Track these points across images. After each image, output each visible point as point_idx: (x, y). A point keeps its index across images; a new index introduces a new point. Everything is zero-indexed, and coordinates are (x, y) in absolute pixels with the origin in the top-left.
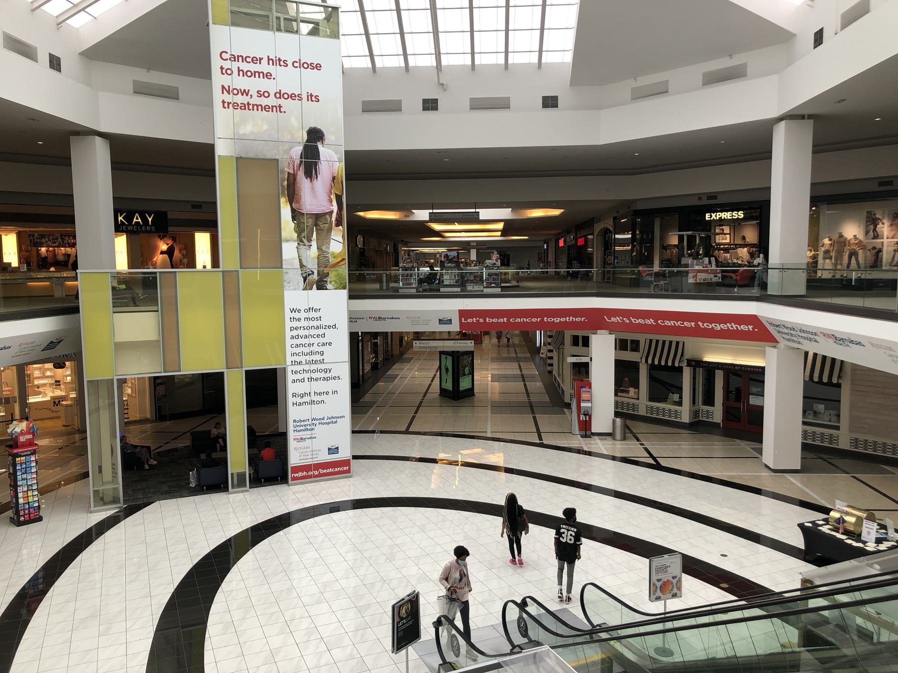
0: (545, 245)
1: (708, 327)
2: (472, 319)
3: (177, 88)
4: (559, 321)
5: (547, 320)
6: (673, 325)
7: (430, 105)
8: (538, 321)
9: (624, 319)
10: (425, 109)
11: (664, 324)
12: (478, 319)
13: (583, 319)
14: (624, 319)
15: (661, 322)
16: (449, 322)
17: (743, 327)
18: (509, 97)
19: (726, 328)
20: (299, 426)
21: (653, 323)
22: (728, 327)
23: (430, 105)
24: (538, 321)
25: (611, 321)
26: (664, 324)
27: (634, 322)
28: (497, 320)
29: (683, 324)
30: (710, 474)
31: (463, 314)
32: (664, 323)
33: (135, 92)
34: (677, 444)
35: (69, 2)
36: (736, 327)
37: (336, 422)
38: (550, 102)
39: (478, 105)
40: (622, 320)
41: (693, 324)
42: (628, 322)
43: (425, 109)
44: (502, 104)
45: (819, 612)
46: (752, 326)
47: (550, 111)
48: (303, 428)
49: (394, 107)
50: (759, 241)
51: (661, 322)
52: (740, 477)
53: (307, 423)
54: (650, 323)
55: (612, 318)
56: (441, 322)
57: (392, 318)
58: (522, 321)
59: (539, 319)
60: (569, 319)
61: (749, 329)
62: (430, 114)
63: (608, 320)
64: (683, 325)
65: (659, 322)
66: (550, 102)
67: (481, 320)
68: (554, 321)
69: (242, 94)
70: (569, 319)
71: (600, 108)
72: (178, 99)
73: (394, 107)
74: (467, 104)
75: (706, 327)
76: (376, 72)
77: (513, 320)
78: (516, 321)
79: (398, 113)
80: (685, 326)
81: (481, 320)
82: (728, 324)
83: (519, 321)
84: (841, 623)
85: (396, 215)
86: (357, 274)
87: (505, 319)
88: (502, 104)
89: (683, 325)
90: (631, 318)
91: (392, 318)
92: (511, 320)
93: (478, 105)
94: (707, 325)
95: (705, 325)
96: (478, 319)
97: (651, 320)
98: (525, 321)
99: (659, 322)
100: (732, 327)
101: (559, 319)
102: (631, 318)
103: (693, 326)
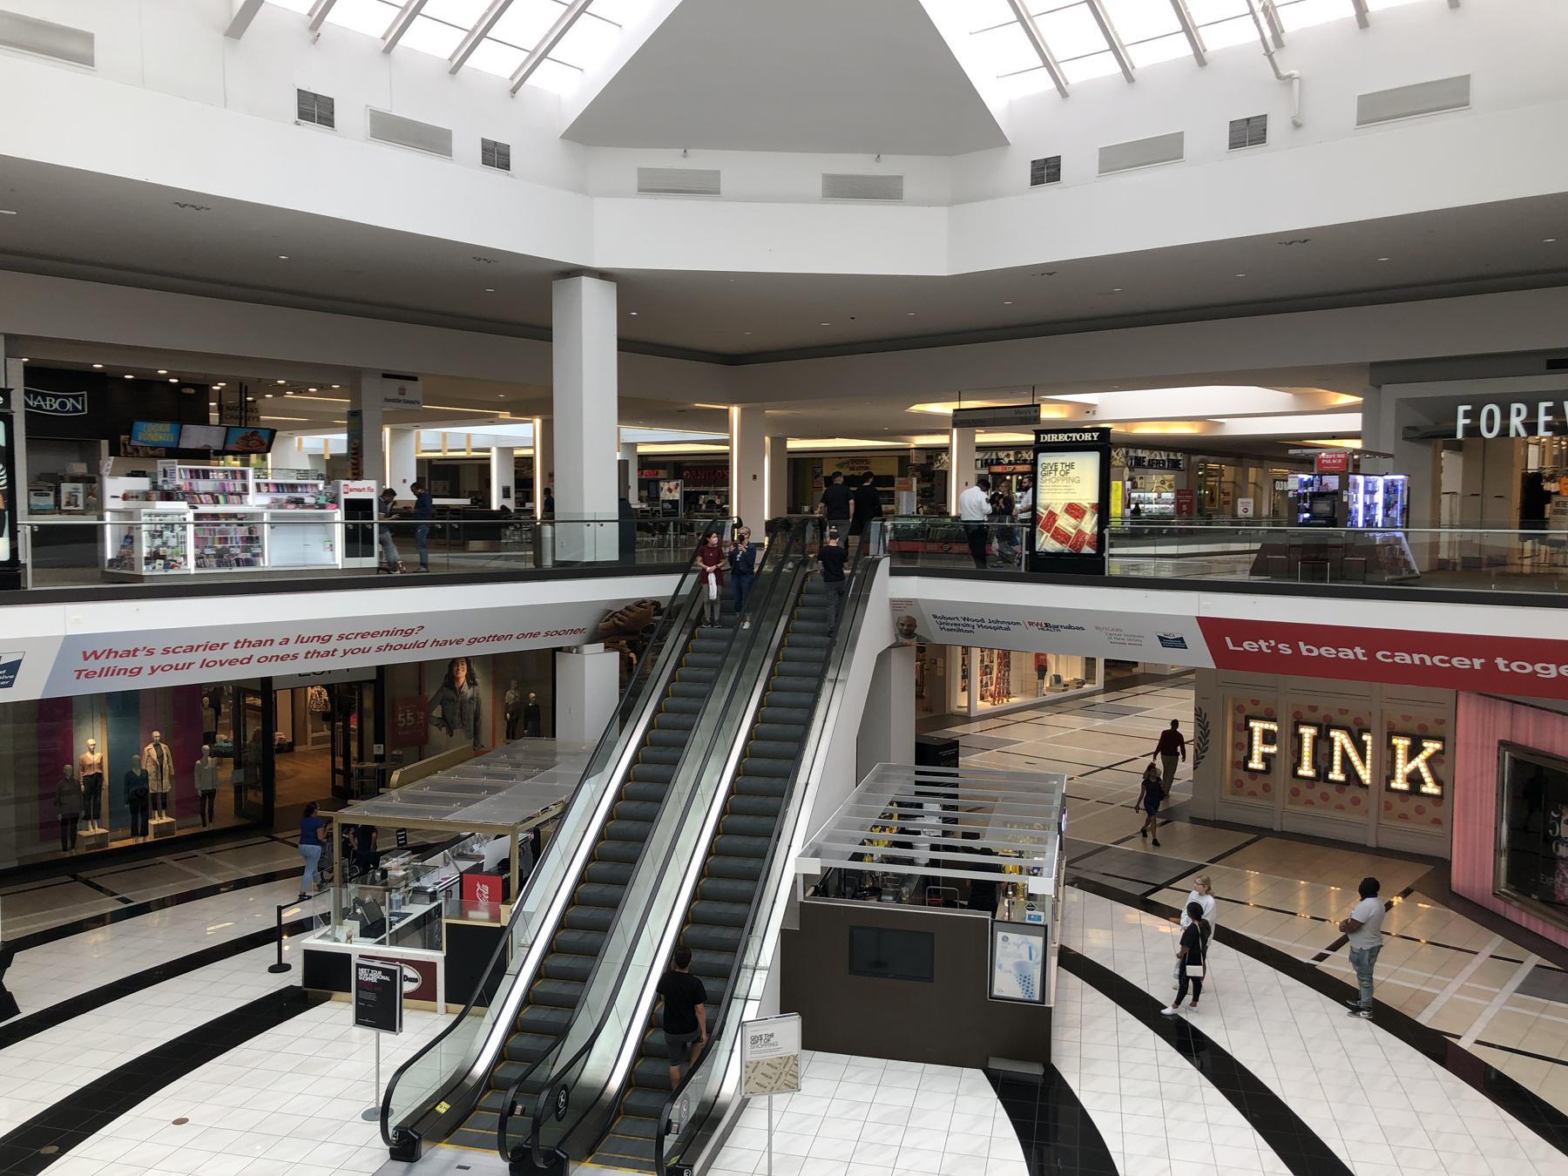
6: (1417, 662)
8: (1477, 667)
9: (1280, 646)
11: (1390, 660)
14: (1280, 646)
15: (1384, 656)
16: (1180, 643)
17: (1347, 654)
19: (1256, 650)
20: (948, 624)
21: (1361, 657)
22: (1260, 647)
25: (1242, 649)
26: (1390, 660)
27: (1305, 653)
30: (1442, 909)
32: (1393, 657)
33: (640, 190)
37: (1008, 629)
40: (1275, 649)
41: (1477, 663)
42: (1289, 652)
45: (664, 1155)
46: (1483, 661)
48: (954, 627)
50: (1280, 38)
51: (1384, 656)
52: (1272, 942)
53: (956, 621)
54: (1352, 657)
55: (1246, 644)
58: (1417, 662)
64: (1447, 665)
65: (1379, 655)
69: (95, 653)
82: (1261, 642)
84: (569, 1086)
89: (1447, 665)
90: (1301, 644)
95: (1514, 666)
99: (1379, 655)
102: (1301, 644)
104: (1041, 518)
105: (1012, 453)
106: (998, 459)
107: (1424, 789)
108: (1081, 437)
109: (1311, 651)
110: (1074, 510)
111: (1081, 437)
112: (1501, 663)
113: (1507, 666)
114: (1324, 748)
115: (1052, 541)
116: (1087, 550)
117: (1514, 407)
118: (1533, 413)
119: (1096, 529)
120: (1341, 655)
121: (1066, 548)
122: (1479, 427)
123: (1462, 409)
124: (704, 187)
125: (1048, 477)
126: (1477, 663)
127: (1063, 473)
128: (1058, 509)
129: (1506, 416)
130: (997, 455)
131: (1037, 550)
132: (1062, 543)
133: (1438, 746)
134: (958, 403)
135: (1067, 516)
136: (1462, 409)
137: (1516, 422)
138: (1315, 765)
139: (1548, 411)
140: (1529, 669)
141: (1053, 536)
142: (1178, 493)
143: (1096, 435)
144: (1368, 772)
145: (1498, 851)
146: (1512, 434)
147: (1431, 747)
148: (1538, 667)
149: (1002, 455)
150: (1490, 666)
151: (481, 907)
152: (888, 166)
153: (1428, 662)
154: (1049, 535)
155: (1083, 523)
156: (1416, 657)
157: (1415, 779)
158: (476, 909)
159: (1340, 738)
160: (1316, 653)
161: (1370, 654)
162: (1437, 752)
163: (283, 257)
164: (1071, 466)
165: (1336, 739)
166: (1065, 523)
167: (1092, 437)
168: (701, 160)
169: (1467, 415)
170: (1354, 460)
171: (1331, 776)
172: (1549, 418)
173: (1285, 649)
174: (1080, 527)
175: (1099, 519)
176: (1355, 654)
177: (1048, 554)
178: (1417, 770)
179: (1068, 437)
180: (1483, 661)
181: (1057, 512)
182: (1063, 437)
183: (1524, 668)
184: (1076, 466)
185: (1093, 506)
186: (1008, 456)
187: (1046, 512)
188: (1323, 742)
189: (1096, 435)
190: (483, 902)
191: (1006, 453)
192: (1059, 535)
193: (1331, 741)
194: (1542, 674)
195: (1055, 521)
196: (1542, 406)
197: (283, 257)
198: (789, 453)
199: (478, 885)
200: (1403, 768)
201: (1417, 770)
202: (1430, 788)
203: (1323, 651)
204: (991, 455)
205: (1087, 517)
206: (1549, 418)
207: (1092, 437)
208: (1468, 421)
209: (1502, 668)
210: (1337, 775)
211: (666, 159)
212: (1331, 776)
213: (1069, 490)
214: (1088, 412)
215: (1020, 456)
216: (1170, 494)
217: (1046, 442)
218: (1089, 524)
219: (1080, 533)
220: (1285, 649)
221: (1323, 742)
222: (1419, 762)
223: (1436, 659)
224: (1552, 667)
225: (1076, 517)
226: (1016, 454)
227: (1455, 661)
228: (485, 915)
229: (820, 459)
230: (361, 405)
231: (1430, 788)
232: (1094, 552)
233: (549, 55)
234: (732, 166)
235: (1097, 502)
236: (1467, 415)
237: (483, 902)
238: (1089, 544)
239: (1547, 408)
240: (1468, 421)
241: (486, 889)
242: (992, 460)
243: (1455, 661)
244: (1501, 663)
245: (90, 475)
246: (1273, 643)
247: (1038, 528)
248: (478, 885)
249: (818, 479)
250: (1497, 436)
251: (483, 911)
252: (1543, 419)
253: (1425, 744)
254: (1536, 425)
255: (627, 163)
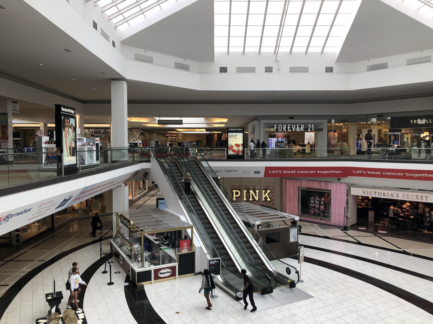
0: (50, 134)
1: (286, 173)
2: (421, 174)
3: (153, 57)
4: (326, 173)
5: (319, 172)
6: (391, 174)
7: (269, 70)
8: (314, 173)
9: (364, 172)
10: (266, 71)
12: (279, 171)
13: (340, 171)
14: (364, 172)
18: (255, 67)
21: (380, 174)
22: (360, 172)
23: (269, 70)
24: (276, 172)
28: (290, 172)
29: (397, 174)
31: (267, 169)
32: (386, 173)
33: (135, 59)
34: (311, 231)
35: (421, 1)
36: (427, 175)
38: (329, 70)
39: (293, 70)
40: (363, 172)
41: (402, 174)
42: (366, 173)
43: (266, 71)
44: (305, 70)
47: (329, 74)
49: (252, 70)
54: (378, 174)
55: (357, 171)
56: (255, 172)
57: (235, 171)
59: (314, 172)
60: (332, 172)
61: (401, 174)
62: (223, 74)
63: (354, 172)
64: (397, 175)
65: (383, 173)
66: (329, 70)
67: (280, 172)
68: (323, 173)
70: (332, 172)
71: (350, 73)
72: (153, 63)
73: (252, 70)
74: (288, 70)
75: (410, 175)
76: (244, 54)
77: (299, 172)
78: (301, 172)
79: (271, 73)
80: (398, 175)
81: (280, 172)
82: (360, 171)
83: (293, 173)
85: (147, 120)
86: (209, 149)
87: (295, 171)
88: (305, 70)
89: (397, 175)
90: (368, 171)
91: (235, 171)
92: (298, 172)
93: (293, 70)
94: (410, 175)
95: (409, 174)
96: (279, 171)
97: (379, 172)
98: (306, 173)
99: (383, 173)
100: (424, 175)
101: (326, 172)
102: (368, 171)
103: (402, 175)
104: (229, 147)
105: (103, 130)
106: (100, 131)
107: (268, 200)
108: (238, 129)
109: (370, 173)
110: (237, 145)
111: (238, 129)
112: (407, 174)
113: (408, 175)
114: (248, 195)
115: (232, 152)
116: (240, 154)
117: (284, 125)
118: (287, 127)
119: (242, 149)
120: (376, 173)
121: (236, 154)
122: (278, 129)
123: (275, 125)
124: (149, 61)
125: (231, 138)
126: (402, 174)
127: (234, 137)
128: (233, 145)
129: (283, 127)
130: (99, 130)
131: (228, 154)
132: (234, 152)
133: (270, 191)
134: (159, 118)
135: (235, 147)
136: (275, 125)
137: (284, 128)
138: (246, 198)
139: (290, 126)
140: (412, 175)
141: (232, 151)
142: (143, 141)
143: (242, 129)
144: (257, 198)
145: (299, 210)
146: (284, 130)
147: (269, 191)
148: (414, 175)
149: (100, 130)
150: (405, 175)
151: (185, 248)
152: (187, 62)
153: (393, 174)
154: (231, 151)
155: (239, 148)
156: (390, 173)
157: (266, 198)
158: (184, 249)
159: (251, 192)
160: (371, 173)
161: (382, 173)
162: (270, 192)
163: (41, 64)
164: (236, 136)
165: (251, 192)
166: (235, 148)
167: (241, 130)
168: (149, 54)
169: (276, 126)
170: (302, 135)
171: (250, 200)
172: (290, 128)
173: (365, 172)
174: (239, 149)
175: (243, 147)
176: (379, 173)
177: (231, 155)
178: (266, 196)
179: (235, 129)
180: (403, 174)
181: (233, 146)
182: (234, 129)
183: (411, 175)
184: (237, 136)
185: (242, 144)
186: (102, 130)
187: (230, 146)
188: (248, 192)
189: (242, 129)
190: (185, 247)
191: (102, 130)
192: (234, 151)
193: (250, 193)
194: (415, 176)
195: (233, 148)
196: (289, 125)
197: (41, 64)
198: (48, 128)
199: (184, 243)
200: (264, 196)
201: (266, 196)
202: (269, 200)
203: (372, 173)
204: (97, 130)
205: (240, 147)
206: (290, 128)
207: (241, 130)
208: (276, 128)
209: (407, 175)
210: (251, 199)
211: (141, 52)
212: (250, 200)
213: (236, 141)
214: (154, 121)
215: (106, 130)
216: (140, 141)
217: (230, 130)
218: (241, 148)
219: (239, 150)
220: (365, 172)
221: (248, 192)
222: (266, 195)
223: (394, 174)
224: (416, 174)
225: (238, 147)
226: (105, 130)
227: (398, 174)
228: (187, 250)
229: (33, 130)
230: (7, 111)
231: (269, 200)
232: (242, 154)
233: (313, 36)
234: (155, 56)
235: (242, 143)
236: (276, 126)
237: (185, 247)
238: (241, 153)
239: (298, 126)
240: (276, 128)
241: (186, 244)
242: (98, 131)
243: (398, 174)
244: (407, 174)
245: (10, 132)
246: (362, 171)
247: (229, 149)
248: (184, 243)
249: (32, 136)
250: (281, 131)
251: (185, 249)
252: (289, 128)
253: (268, 191)
254: (288, 129)
255: (134, 51)
